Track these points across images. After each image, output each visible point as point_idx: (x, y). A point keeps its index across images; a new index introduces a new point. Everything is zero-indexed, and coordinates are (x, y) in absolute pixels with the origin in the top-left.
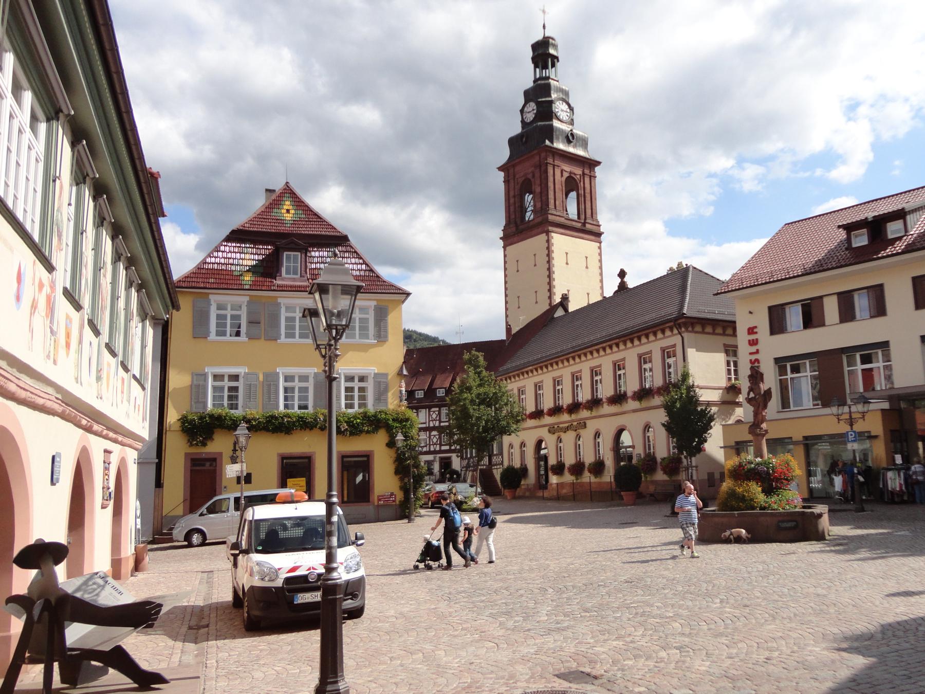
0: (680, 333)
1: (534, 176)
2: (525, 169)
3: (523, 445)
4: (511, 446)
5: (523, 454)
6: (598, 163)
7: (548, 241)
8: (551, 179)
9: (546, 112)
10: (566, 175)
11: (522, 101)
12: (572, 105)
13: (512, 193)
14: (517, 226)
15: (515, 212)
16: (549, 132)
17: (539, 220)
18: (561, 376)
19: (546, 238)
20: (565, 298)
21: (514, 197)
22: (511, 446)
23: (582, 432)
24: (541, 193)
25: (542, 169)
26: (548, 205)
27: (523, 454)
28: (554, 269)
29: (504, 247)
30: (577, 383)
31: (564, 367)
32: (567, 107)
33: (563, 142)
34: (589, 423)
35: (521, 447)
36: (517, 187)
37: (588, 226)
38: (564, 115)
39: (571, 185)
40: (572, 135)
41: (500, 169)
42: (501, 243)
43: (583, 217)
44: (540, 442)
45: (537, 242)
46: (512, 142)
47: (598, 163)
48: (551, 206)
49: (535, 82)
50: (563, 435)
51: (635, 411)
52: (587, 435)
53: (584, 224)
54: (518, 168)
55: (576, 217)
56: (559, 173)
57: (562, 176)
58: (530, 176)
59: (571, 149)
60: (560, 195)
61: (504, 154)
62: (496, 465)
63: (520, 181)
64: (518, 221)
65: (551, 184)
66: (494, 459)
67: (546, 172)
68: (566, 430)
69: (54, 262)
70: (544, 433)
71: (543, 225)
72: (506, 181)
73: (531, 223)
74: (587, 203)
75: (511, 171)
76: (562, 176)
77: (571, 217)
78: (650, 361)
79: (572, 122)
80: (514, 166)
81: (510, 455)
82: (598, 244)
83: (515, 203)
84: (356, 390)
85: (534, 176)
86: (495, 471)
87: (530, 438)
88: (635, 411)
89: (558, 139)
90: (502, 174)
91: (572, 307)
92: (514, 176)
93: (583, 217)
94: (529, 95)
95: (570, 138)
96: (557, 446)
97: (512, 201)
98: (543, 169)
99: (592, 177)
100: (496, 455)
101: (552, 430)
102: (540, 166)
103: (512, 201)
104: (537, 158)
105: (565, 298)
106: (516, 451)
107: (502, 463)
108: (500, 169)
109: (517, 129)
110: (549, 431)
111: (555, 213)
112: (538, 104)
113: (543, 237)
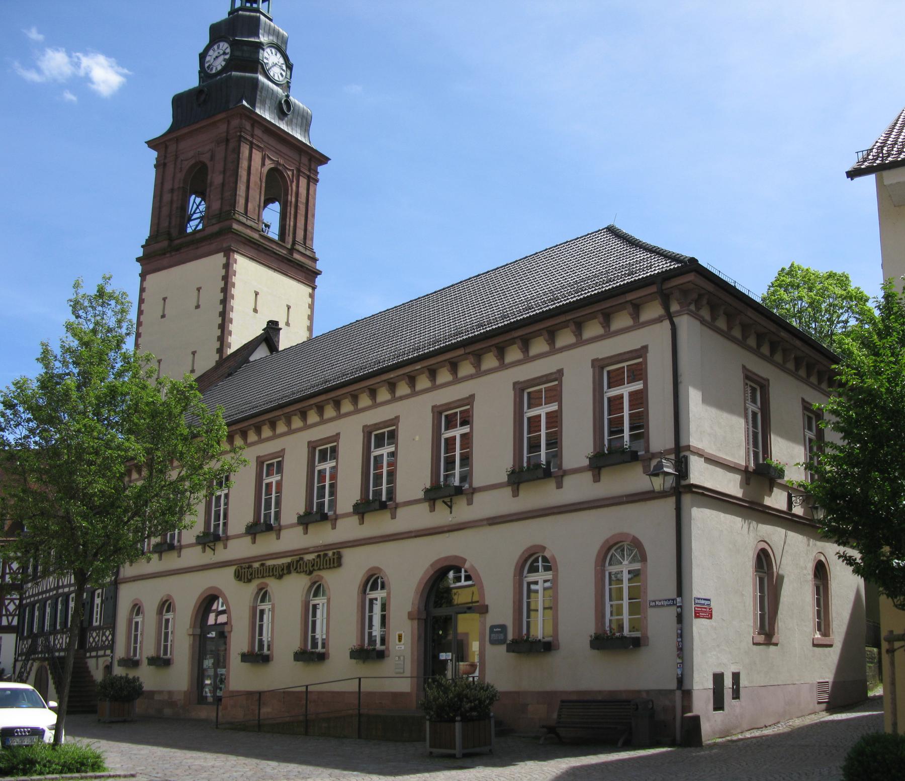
0: (670, 316)
1: (212, 158)
2: (201, 145)
3: (166, 605)
4: (137, 609)
5: (163, 627)
6: (324, 160)
7: (227, 266)
8: (244, 164)
9: (247, 59)
10: (269, 165)
11: (206, 41)
12: (292, 61)
13: (168, 186)
14: (171, 240)
15: (170, 216)
16: (252, 90)
17: (216, 228)
18: (281, 453)
19: (224, 260)
20: (272, 328)
21: (172, 191)
22: (137, 609)
23: (329, 577)
24: (223, 185)
25: (231, 146)
26: (234, 204)
27: (163, 627)
28: (233, 315)
29: (143, 276)
30: (319, 467)
31: (291, 432)
32: (282, 61)
33: (271, 112)
34: (348, 555)
35: (160, 612)
36: (180, 176)
37: (296, 256)
38: (276, 73)
39: (275, 188)
40: (288, 102)
41: (152, 144)
42: (138, 268)
43: (289, 239)
44: (208, 601)
45: (205, 269)
46: (179, 102)
47: (324, 160)
48: (240, 207)
49: (229, 14)
50: (273, 584)
51: (493, 521)
52: (343, 583)
53: (292, 250)
54: (183, 145)
55: (276, 238)
56: (256, 164)
57: (263, 164)
58: (205, 158)
59: (283, 126)
60: (256, 196)
61: (162, 121)
62: (97, 649)
63: (187, 165)
64: (174, 232)
65: (243, 173)
66: (93, 638)
67: (237, 151)
68: (281, 573)
69: (710, 685)
70: (224, 580)
71: (225, 236)
72: (160, 166)
73: (198, 236)
74: (297, 216)
75: (172, 148)
76: (263, 164)
77: (270, 235)
78: (464, 423)
79: (287, 86)
80: (178, 140)
81: (133, 628)
82: (310, 290)
83: (172, 202)
84: (626, 577)
85: (212, 158)
86: (91, 663)
87: (187, 593)
88: (493, 521)
89: (263, 103)
90: (154, 154)
91: (286, 341)
92: (177, 157)
93: (289, 239)
94: (218, 33)
95: (284, 108)
96: (254, 609)
97: (167, 197)
98: (232, 145)
99: (313, 180)
100: (99, 628)
101: (245, 571)
102: (227, 140)
103: (167, 197)
104: (223, 128)
105: (272, 328)
106: (148, 621)
107: (112, 647)
108: (152, 144)
109: (193, 82)
110: (239, 576)
111: (244, 220)
112: (234, 45)
113: (220, 258)
